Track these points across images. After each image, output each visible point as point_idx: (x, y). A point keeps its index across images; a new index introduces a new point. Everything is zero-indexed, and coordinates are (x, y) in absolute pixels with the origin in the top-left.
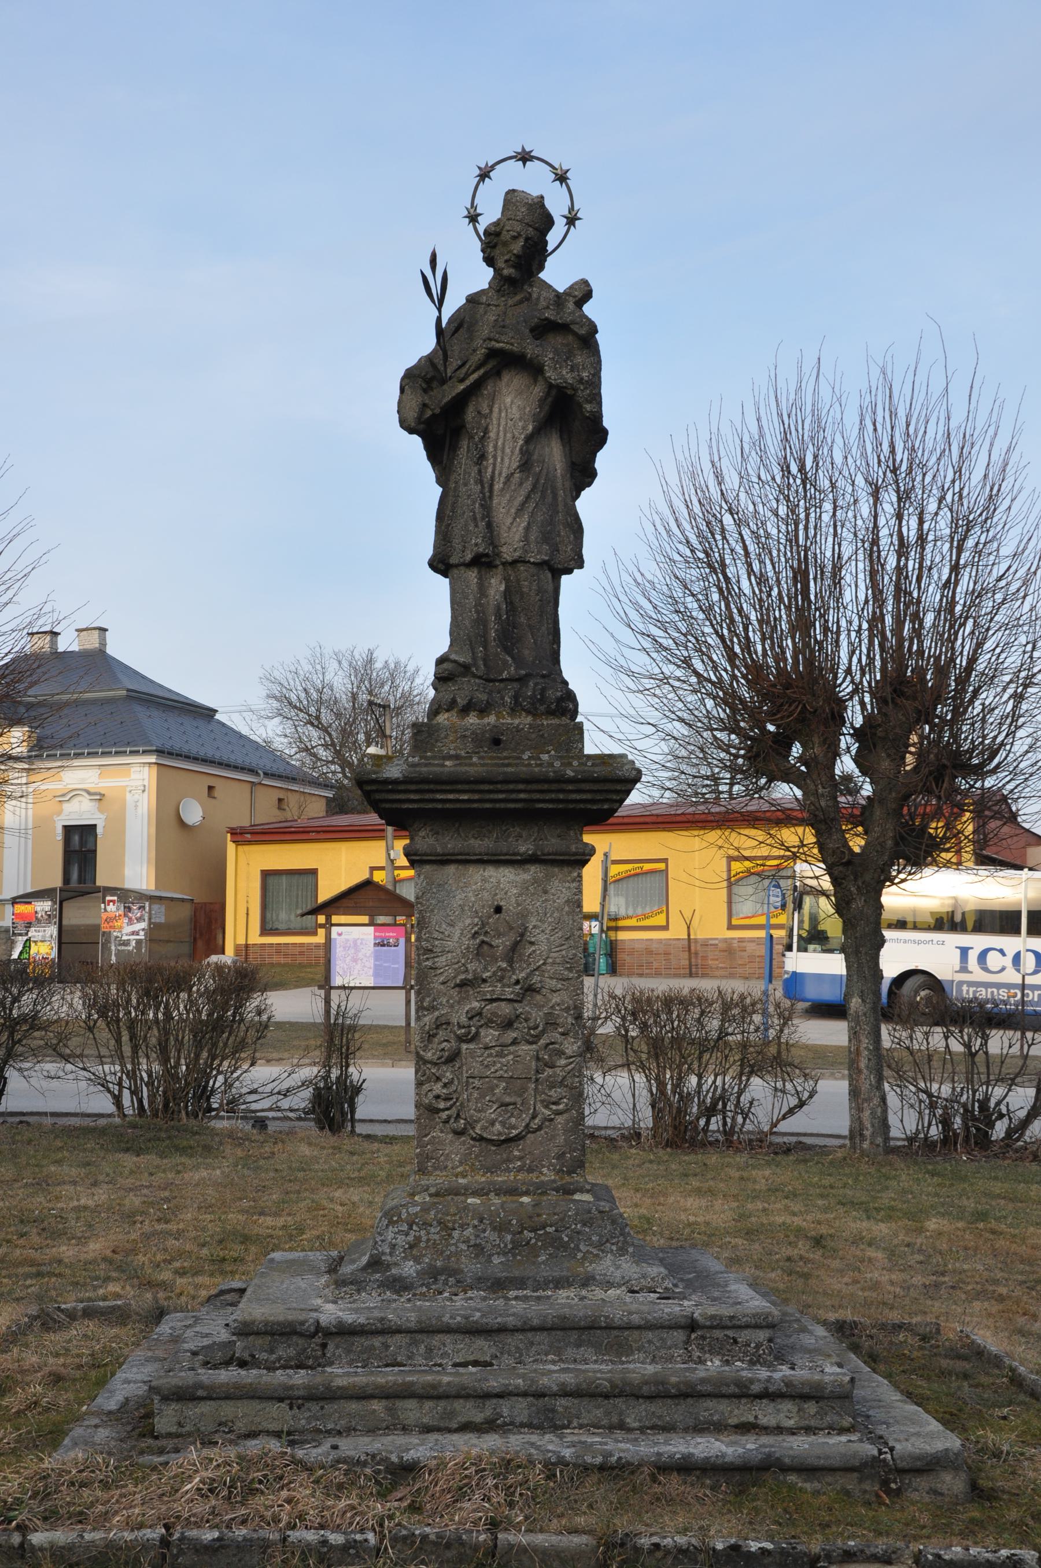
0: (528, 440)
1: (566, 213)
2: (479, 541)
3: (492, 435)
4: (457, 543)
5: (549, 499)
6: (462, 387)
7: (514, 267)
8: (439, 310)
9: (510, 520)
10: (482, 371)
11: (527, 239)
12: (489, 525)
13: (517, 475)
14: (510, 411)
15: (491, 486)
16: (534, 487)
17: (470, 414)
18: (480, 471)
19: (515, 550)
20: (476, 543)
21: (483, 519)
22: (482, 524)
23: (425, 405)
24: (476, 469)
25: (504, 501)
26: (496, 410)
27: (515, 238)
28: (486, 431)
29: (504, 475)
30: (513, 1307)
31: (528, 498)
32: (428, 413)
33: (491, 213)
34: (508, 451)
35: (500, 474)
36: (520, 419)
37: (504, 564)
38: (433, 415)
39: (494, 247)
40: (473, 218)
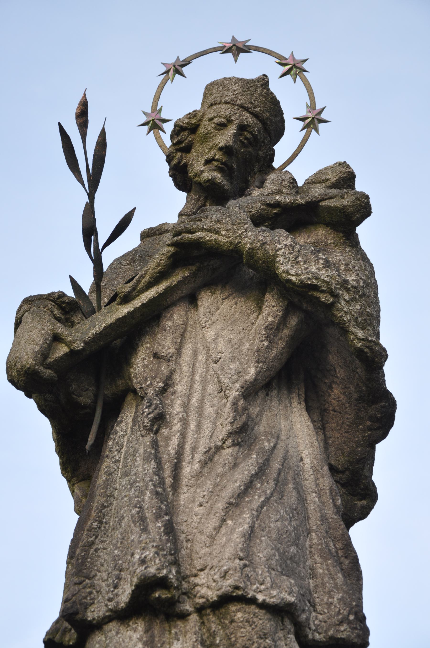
0: (250, 392)
1: (303, 113)
2: (150, 553)
3: (180, 388)
4: (102, 579)
5: (291, 497)
6: (125, 310)
7: (219, 170)
8: (91, 195)
9: (214, 522)
10: (163, 286)
11: (242, 128)
12: (170, 529)
13: (227, 452)
14: (217, 346)
15: (177, 468)
16: (260, 473)
17: (141, 364)
18: (155, 444)
19: (224, 576)
20: (144, 558)
21: (158, 517)
22: (156, 527)
23: (57, 338)
24: (148, 440)
25: (201, 494)
26: (187, 351)
27: (222, 126)
28: (168, 383)
29: (202, 449)
30: (105, 512)
31: (249, 486)
32: (62, 350)
33: (183, 101)
34: (209, 410)
35: (194, 449)
36: (233, 359)
37: (200, 610)
38: (73, 353)
39: (187, 149)
40: (154, 125)
